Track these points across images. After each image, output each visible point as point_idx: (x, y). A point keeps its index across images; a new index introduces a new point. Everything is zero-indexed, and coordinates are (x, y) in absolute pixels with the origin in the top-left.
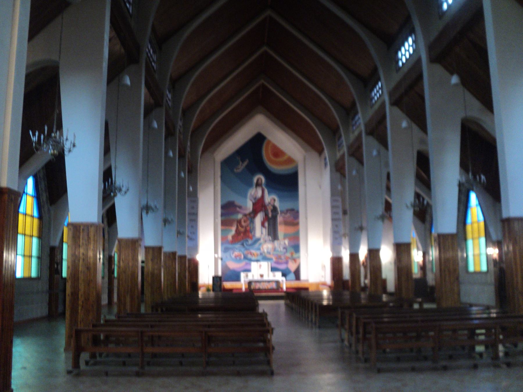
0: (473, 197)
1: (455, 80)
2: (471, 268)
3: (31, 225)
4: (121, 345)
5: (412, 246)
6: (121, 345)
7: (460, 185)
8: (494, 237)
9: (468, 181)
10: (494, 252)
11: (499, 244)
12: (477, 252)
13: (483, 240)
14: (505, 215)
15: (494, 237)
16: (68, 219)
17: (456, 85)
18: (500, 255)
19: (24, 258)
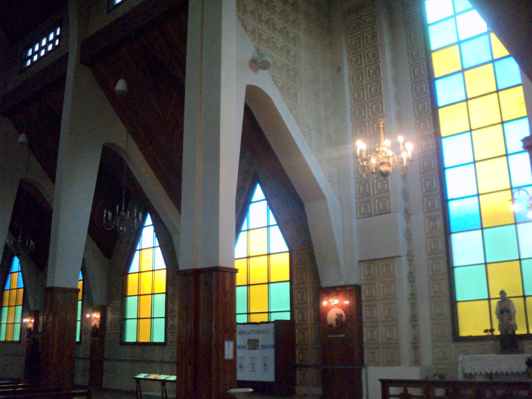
0: (16, 261)
1: (22, 138)
2: (130, 337)
3: (250, 307)
4: (512, 322)
5: (40, 313)
6: (512, 322)
7: (6, 247)
8: (32, 307)
9: (15, 245)
10: (29, 321)
11: (35, 314)
12: (11, 321)
13: (19, 309)
14: (49, 285)
15: (32, 307)
16: (11, 276)
17: (23, 144)
18: (36, 324)
19: (3, 307)
